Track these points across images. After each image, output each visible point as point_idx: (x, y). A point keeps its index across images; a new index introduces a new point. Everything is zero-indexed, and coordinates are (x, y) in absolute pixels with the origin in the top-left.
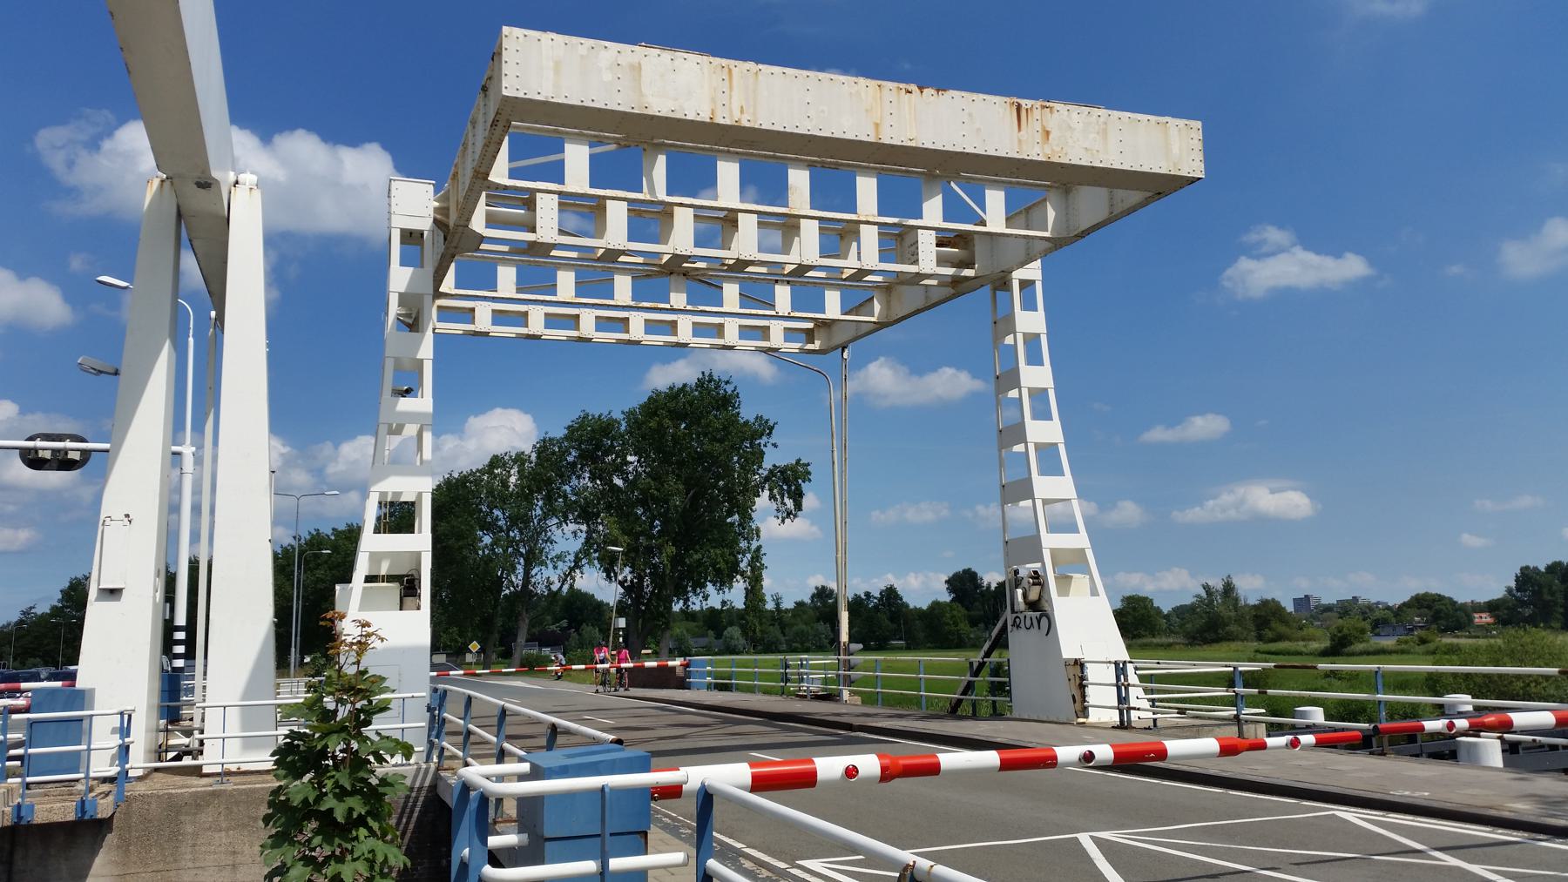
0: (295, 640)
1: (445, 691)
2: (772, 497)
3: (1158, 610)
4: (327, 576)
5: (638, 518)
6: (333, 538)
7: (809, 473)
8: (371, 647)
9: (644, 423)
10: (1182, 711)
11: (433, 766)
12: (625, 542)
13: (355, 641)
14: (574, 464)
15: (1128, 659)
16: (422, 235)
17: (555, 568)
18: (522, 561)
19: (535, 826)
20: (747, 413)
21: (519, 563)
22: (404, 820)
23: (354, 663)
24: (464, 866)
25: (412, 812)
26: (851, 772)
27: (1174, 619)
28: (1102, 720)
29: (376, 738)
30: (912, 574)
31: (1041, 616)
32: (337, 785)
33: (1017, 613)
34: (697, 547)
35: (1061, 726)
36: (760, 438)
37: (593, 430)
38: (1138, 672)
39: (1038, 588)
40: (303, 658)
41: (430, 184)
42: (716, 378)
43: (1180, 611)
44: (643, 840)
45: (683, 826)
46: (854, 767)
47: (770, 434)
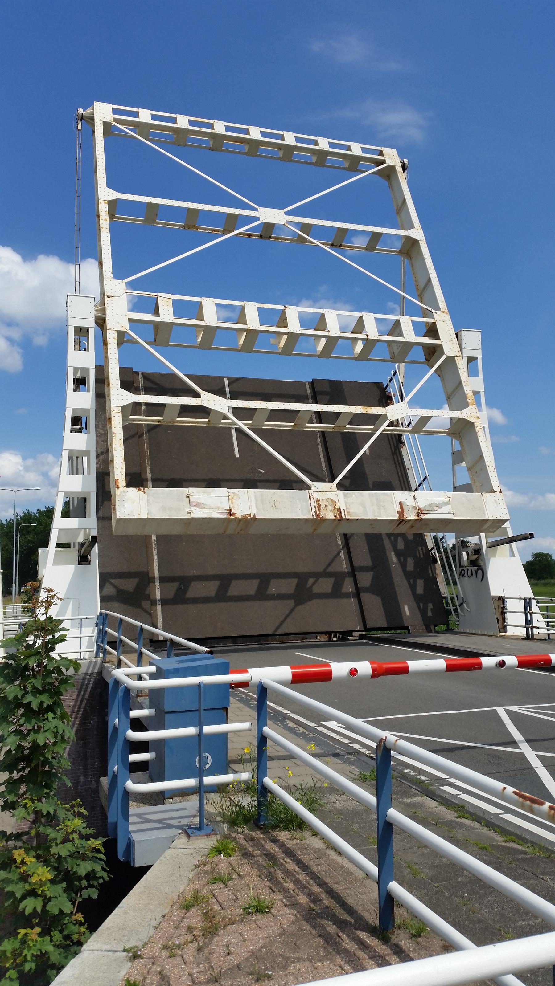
0: (15, 579)
1: (107, 615)
4: (34, 538)
6: (37, 515)
8: (54, 603)
11: (99, 660)
13: (44, 600)
15: (533, 597)
16: (88, 330)
19: (159, 704)
22: (82, 693)
23: (43, 614)
24: (116, 729)
25: (87, 687)
26: (353, 672)
28: (516, 634)
29: (59, 658)
31: (478, 570)
32: (34, 687)
35: (489, 638)
38: (538, 605)
40: (20, 589)
44: (225, 713)
45: (252, 699)
46: (355, 669)
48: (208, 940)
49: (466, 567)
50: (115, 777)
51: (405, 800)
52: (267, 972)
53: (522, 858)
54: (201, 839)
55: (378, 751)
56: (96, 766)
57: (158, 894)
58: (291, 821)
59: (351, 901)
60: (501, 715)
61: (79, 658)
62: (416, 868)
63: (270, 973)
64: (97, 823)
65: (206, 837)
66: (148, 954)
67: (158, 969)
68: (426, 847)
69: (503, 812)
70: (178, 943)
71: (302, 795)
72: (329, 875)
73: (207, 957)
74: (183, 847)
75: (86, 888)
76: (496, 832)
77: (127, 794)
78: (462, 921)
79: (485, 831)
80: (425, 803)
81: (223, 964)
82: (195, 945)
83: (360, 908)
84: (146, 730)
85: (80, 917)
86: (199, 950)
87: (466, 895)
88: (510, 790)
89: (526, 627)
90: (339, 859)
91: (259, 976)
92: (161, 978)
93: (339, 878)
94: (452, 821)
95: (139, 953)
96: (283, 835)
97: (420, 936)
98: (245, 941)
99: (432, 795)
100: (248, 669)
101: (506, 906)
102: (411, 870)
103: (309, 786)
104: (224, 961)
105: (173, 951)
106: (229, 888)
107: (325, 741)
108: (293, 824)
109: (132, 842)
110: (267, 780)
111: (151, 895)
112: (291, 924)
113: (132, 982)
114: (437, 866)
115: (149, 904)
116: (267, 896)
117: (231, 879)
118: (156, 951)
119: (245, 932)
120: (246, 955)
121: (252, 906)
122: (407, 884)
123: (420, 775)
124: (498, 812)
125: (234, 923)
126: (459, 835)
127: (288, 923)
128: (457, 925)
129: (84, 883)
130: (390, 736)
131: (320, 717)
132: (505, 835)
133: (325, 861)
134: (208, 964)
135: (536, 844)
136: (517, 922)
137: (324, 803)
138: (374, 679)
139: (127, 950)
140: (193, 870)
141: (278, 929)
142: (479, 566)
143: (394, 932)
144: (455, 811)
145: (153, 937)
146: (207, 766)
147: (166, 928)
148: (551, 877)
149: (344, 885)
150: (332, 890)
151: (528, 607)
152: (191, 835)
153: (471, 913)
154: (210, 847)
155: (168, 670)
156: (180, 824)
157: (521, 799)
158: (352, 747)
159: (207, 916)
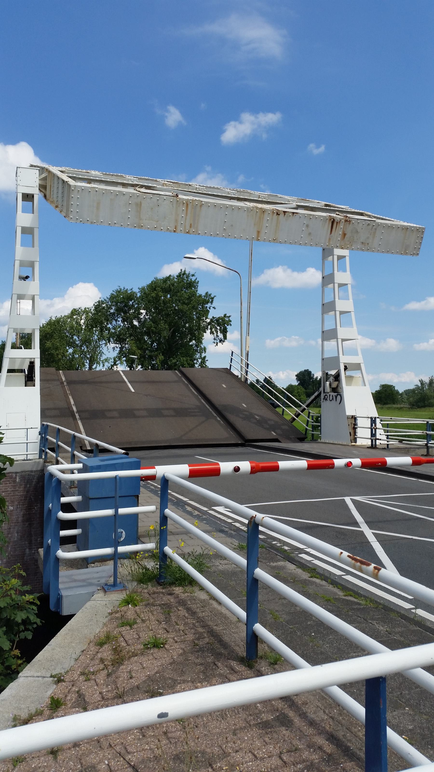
1: (47, 426)
2: (212, 333)
3: (397, 392)
5: (146, 341)
7: (231, 321)
9: (149, 294)
10: (401, 441)
12: (139, 353)
14: (113, 314)
15: (377, 416)
16: (33, 196)
17: (104, 366)
18: (88, 361)
20: (201, 291)
21: (87, 362)
24: (50, 511)
26: (237, 469)
27: (405, 396)
28: (363, 444)
30: (281, 372)
31: (337, 395)
33: (326, 393)
34: (174, 356)
35: (343, 446)
36: (207, 303)
37: (123, 297)
38: (381, 422)
39: (336, 383)
41: (37, 169)
42: (187, 272)
43: (407, 392)
44: (137, 499)
47: (212, 302)
48: (116, 668)
49: (328, 393)
50: (49, 547)
51: (272, 564)
52: (159, 690)
53: (357, 608)
54: (114, 593)
55: (249, 525)
56: (39, 542)
57: (79, 635)
58: (184, 580)
59: (226, 639)
60: (347, 503)
61: (26, 459)
62: (276, 614)
63: (161, 691)
64: (39, 585)
65: (120, 592)
66: (69, 678)
67: (75, 689)
68: (285, 598)
69: (345, 574)
70: (92, 670)
71: (193, 560)
72: (211, 619)
73: (114, 681)
74: (100, 599)
75: (23, 631)
76: (338, 589)
77: (57, 560)
78: (309, 653)
79: (331, 587)
80: (286, 566)
81: (126, 685)
82: (105, 672)
83: (233, 644)
84: (75, 511)
85: (17, 652)
86: (109, 675)
87: (313, 634)
88: (346, 554)
89: (371, 439)
90: (219, 607)
91: (153, 693)
92: (78, 696)
93: (218, 621)
94: (306, 580)
95: (62, 678)
96: (178, 590)
97: (276, 664)
98: (144, 668)
99: (292, 560)
100: (155, 467)
101: (342, 642)
102: (273, 615)
103: (197, 553)
104: (127, 683)
105: (88, 676)
106: (134, 630)
107: (214, 521)
108: (186, 581)
109: (61, 596)
110: (167, 549)
111: (74, 636)
112: (179, 655)
113: (56, 699)
114: (292, 613)
115: (71, 642)
116: (162, 635)
117: (136, 623)
118: (76, 676)
119: (144, 661)
120: (144, 678)
121: (150, 643)
122: (269, 626)
123: (284, 545)
124: (341, 574)
125: (136, 656)
126: (311, 590)
127: (177, 655)
128: (305, 656)
129: (22, 627)
130: (259, 516)
131: (211, 503)
132: (345, 591)
133: (209, 609)
134: (114, 685)
135: (368, 598)
136: (350, 654)
137: (210, 566)
138: (252, 475)
139: (53, 676)
140: (106, 617)
141: (169, 659)
142: (338, 392)
143: (257, 661)
144: (308, 572)
145: (73, 666)
146: (122, 539)
147: (84, 660)
148: (378, 622)
149: (221, 627)
150: (212, 630)
151: (374, 424)
152: (107, 590)
153: (316, 647)
154: (121, 600)
155: (92, 466)
156: (99, 582)
157: (353, 562)
158: (235, 526)
159: (116, 651)
